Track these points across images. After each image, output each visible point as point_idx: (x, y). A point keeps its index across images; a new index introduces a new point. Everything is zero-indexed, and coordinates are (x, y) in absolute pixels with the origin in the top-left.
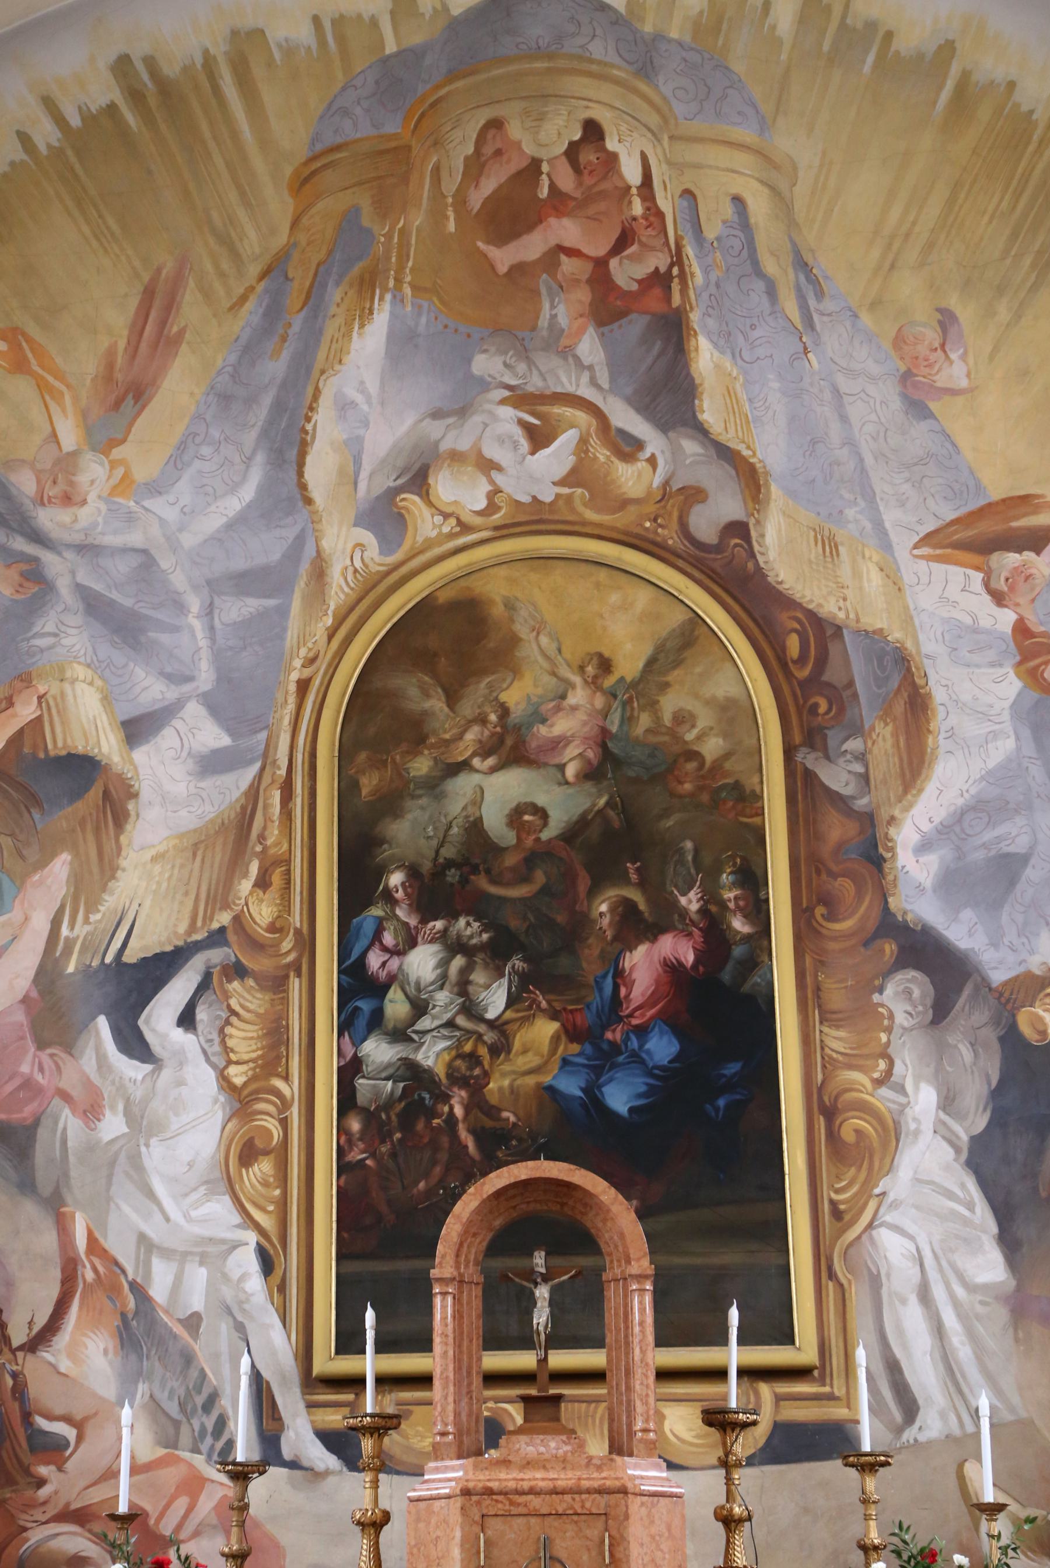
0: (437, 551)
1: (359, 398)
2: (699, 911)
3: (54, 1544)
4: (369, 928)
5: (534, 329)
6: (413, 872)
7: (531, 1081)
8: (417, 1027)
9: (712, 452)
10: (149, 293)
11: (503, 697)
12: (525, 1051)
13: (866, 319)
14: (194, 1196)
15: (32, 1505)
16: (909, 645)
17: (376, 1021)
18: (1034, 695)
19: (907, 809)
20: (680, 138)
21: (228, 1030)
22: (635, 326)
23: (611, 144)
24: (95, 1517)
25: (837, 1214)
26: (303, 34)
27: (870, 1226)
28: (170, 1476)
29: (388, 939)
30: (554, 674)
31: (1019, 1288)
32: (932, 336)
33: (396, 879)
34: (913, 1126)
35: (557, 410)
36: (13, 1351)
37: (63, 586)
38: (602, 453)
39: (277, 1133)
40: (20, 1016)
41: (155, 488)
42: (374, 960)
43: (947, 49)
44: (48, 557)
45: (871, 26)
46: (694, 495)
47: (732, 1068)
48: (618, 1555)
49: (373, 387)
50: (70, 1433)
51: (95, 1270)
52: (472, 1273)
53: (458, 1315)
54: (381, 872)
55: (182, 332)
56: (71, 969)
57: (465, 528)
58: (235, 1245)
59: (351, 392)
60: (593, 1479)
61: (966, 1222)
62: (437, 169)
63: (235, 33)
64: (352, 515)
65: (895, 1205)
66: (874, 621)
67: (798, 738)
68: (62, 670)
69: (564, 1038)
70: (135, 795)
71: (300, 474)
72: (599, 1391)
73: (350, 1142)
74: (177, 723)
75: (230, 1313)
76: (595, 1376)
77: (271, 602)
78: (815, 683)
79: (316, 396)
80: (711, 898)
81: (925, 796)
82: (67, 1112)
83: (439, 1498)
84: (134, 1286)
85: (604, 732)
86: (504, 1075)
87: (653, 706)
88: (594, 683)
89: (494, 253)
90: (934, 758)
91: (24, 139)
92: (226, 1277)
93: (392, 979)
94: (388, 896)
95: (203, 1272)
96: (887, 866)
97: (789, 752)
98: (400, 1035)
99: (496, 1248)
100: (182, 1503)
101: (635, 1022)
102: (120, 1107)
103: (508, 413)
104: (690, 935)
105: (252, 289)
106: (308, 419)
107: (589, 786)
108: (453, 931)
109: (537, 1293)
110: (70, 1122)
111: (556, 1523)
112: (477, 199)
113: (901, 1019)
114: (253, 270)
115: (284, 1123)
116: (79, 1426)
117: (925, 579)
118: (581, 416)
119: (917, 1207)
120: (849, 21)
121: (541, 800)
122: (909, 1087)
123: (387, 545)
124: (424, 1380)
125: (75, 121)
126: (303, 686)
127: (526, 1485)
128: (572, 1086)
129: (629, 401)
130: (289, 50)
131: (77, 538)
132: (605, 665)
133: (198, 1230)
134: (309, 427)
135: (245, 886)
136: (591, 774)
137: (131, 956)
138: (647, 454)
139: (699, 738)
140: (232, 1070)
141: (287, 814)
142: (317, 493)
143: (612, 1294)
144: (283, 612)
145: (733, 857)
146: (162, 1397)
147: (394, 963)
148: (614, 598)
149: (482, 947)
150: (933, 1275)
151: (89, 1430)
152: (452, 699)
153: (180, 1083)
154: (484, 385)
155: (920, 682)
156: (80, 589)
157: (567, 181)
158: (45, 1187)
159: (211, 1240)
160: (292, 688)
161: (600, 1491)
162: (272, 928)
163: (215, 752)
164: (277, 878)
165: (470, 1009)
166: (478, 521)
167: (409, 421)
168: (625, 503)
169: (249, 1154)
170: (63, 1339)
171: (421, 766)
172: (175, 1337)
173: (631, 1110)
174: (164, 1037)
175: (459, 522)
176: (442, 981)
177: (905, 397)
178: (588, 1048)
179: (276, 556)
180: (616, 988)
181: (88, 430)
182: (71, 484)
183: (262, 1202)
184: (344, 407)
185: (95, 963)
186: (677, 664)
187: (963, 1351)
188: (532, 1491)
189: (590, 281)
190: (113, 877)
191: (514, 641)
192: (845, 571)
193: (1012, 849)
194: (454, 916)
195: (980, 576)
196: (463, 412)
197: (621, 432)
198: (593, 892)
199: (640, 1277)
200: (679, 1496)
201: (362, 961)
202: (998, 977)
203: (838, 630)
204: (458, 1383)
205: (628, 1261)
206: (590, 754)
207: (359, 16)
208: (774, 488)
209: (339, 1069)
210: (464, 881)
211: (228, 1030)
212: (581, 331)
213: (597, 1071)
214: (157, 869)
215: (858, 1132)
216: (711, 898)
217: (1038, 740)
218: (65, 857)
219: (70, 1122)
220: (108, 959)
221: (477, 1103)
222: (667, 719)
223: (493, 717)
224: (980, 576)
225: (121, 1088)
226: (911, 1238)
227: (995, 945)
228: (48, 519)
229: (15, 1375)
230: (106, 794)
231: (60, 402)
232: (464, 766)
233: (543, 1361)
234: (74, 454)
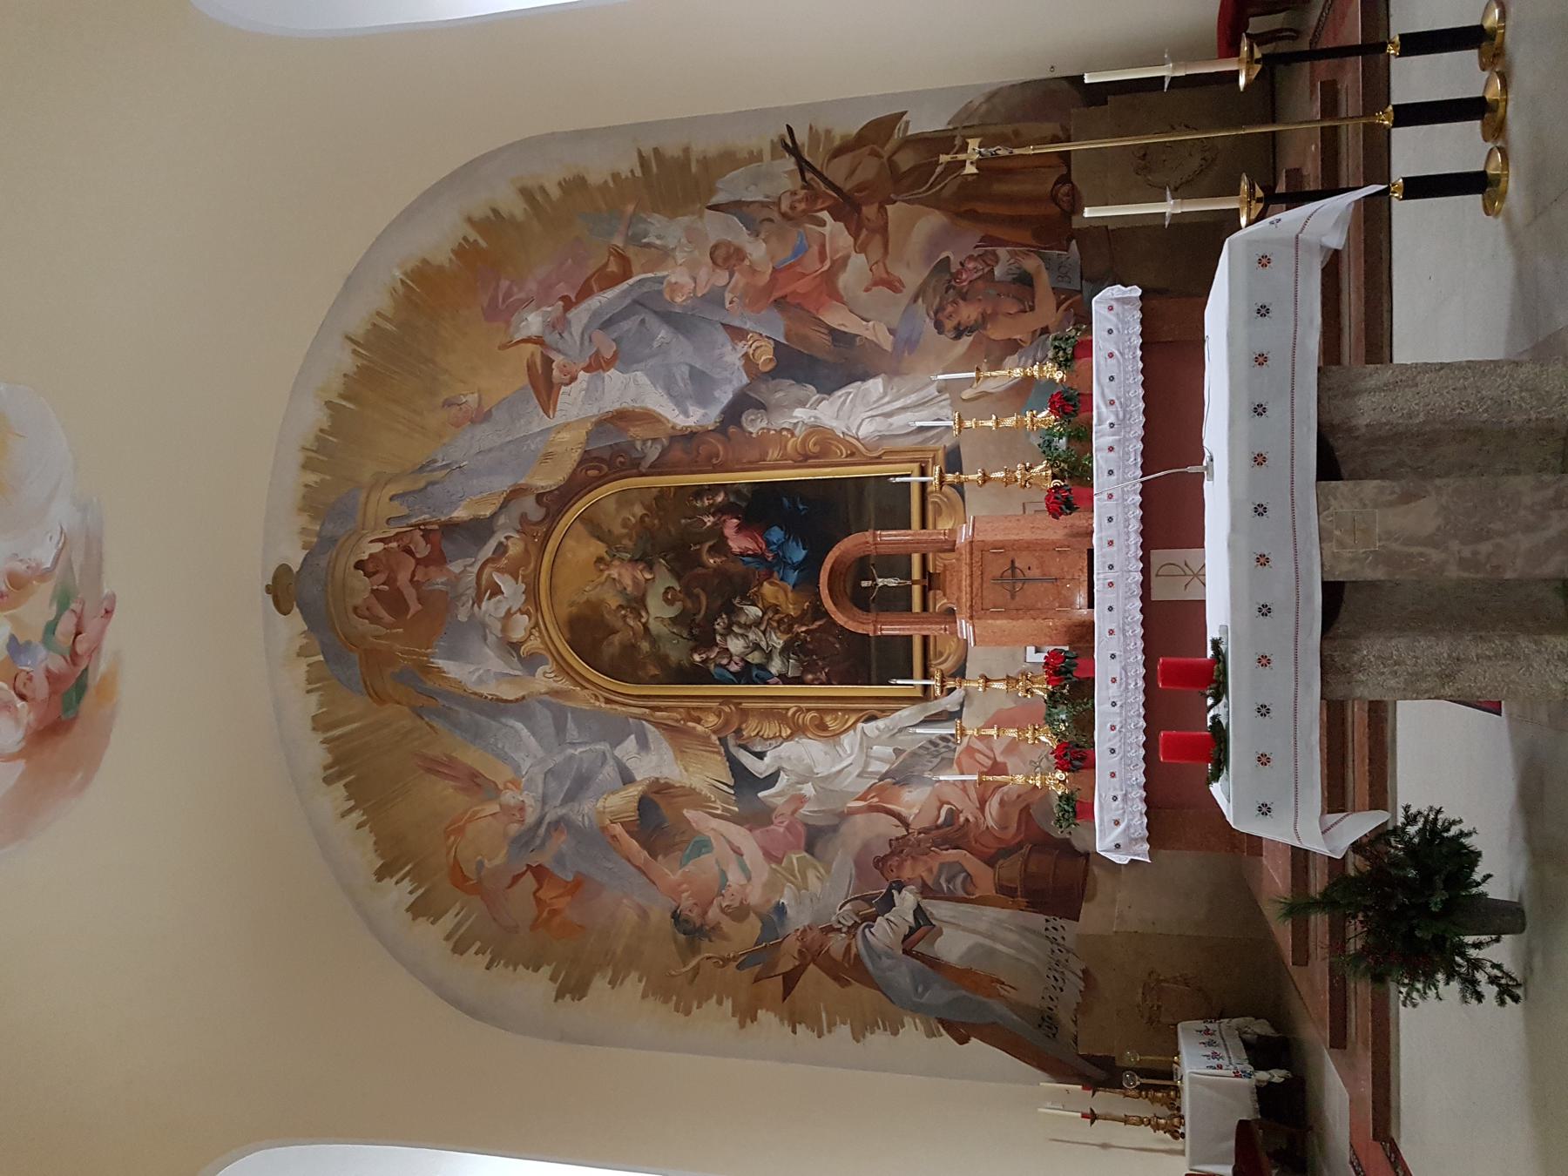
0: (547, 638)
1: (477, 674)
2: (714, 516)
3: (994, 813)
5: (447, 593)
6: (694, 650)
7: (790, 595)
8: (765, 648)
9: (504, 510)
10: (429, 770)
11: (614, 607)
12: (777, 598)
13: (446, 440)
14: (841, 752)
15: (977, 824)
16: (593, 420)
17: (763, 667)
18: (617, 363)
19: (668, 421)
20: (363, 524)
21: (765, 736)
22: (447, 547)
23: (365, 557)
24: (983, 796)
25: (852, 454)
26: (314, 697)
27: (858, 439)
28: (965, 761)
29: (725, 662)
30: (603, 584)
31: (885, 373)
32: (455, 410)
33: (697, 658)
34: (812, 419)
35: (484, 582)
36: (909, 833)
37: (562, 811)
38: (504, 561)
39: (813, 714)
40: (758, 832)
41: (517, 768)
42: (734, 668)
43: (328, 404)
44: (548, 819)
45: (317, 438)
46: (523, 518)
48: (1001, 544)
49: (472, 668)
50: (946, 807)
51: (873, 797)
52: (872, 616)
53: (891, 623)
54: (693, 664)
55: (446, 756)
56: (736, 809)
57: (536, 625)
59: (474, 677)
60: (966, 557)
61: (856, 395)
62: (377, 637)
63: (314, 729)
64: (530, 678)
65: (848, 428)
66: (582, 434)
67: (635, 471)
68: (599, 812)
69: (772, 580)
70: (657, 779)
71: (511, 701)
72: (930, 556)
73: (818, 679)
74: (624, 760)
78: (610, 463)
79: (475, 694)
80: (707, 511)
81: (662, 413)
82: (801, 811)
83: (974, 632)
84: (880, 780)
85: (630, 560)
86: (788, 608)
88: (608, 565)
89: (412, 612)
90: (646, 409)
91: (360, 826)
92: (878, 736)
93: (743, 660)
95: (875, 747)
96: (694, 430)
98: (769, 656)
99: (866, 609)
100: (979, 756)
101: (764, 547)
102: (800, 786)
103: (484, 605)
104: (725, 521)
105: (427, 723)
106: (486, 697)
107: (656, 567)
108: (721, 631)
109: (881, 584)
110: (805, 810)
111: (985, 574)
112: (387, 618)
113: (764, 424)
114: (419, 722)
115: (809, 710)
116: (942, 803)
117: (564, 413)
118: (487, 571)
119: (849, 418)
120: (314, 448)
122: (795, 421)
125: (352, 803)
126: (608, 701)
127: (968, 589)
128: (793, 576)
129: (480, 549)
130: (321, 705)
131: (539, 804)
132: (600, 560)
133: (856, 749)
134: (490, 697)
135: (699, 728)
136: (650, 567)
137: (731, 782)
138: (503, 540)
139: (634, 516)
140: (784, 735)
141: (666, 709)
143: (883, 550)
144: (574, 710)
145: (689, 501)
146: (931, 765)
148: (569, 555)
149: (729, 618)
150: (879, 411)
151: (944, 799)
152: (615, 632)
153: (789, 758)
154: (472, 616)
155: (610, 414)
156: (564, 802)
157: (382, 577)
158: (836, 821)
159: (861, 744)
160: (608, 706)
161: (971, 554)
162: (719, 716)
164: (695, 714)
165: (757, 623)
166: (533, 619)
167: (488, 651)
168: (526, 551)
169: (822, 727)
170: (904, 811)
171: (645, 646)
172: (904, 759)
173: (804, 549)
174: (768, 766)
175: (534, 628)
176: (744, 636)
177: (481, 422)
178: (776, 568)
179: (548, 713)
180: (749, 555)
181: (490, 800)
182: (514, 807)
183: (844, 721)
184: (480, 681)
185: (734, 798)
186: (599, 526)
187: (913, 398)
188: (971, 586)
189: (426, 566)
190: (694, 789)
193: (687, 373)
195: (563, 387)
196: (484, 626)
197: (494, 553)
198: (703, 566)
199: (875, 536)
200: (974, 518)
202: (745, 380)
204: (923, 623)
205: (867, 543)
206: (641, 567)
207: (307, 671)
208: (522, 481)
209: (784, 684)
210: (698, 626)
211: (765, 736)
212: (449, 571)
213: (786, 564)
214: (691, 769)
215: (815, 445)
216: (707, 511)
217: (638, 361)
218: (685, 812)
219: (805, 810)
220: (732, 792)
221: (800, 620)
222: (625, 531)
223: (623, 612)
224: (563, 387)
225: (791, 785)
226: (863, 420)
227: (731, 382)
228: (531, 818)
229: (919, 833)
230: (656, 792)
231: (478, 812)
232: (645, 625)
233: (915, 582)
234: (501, 806)
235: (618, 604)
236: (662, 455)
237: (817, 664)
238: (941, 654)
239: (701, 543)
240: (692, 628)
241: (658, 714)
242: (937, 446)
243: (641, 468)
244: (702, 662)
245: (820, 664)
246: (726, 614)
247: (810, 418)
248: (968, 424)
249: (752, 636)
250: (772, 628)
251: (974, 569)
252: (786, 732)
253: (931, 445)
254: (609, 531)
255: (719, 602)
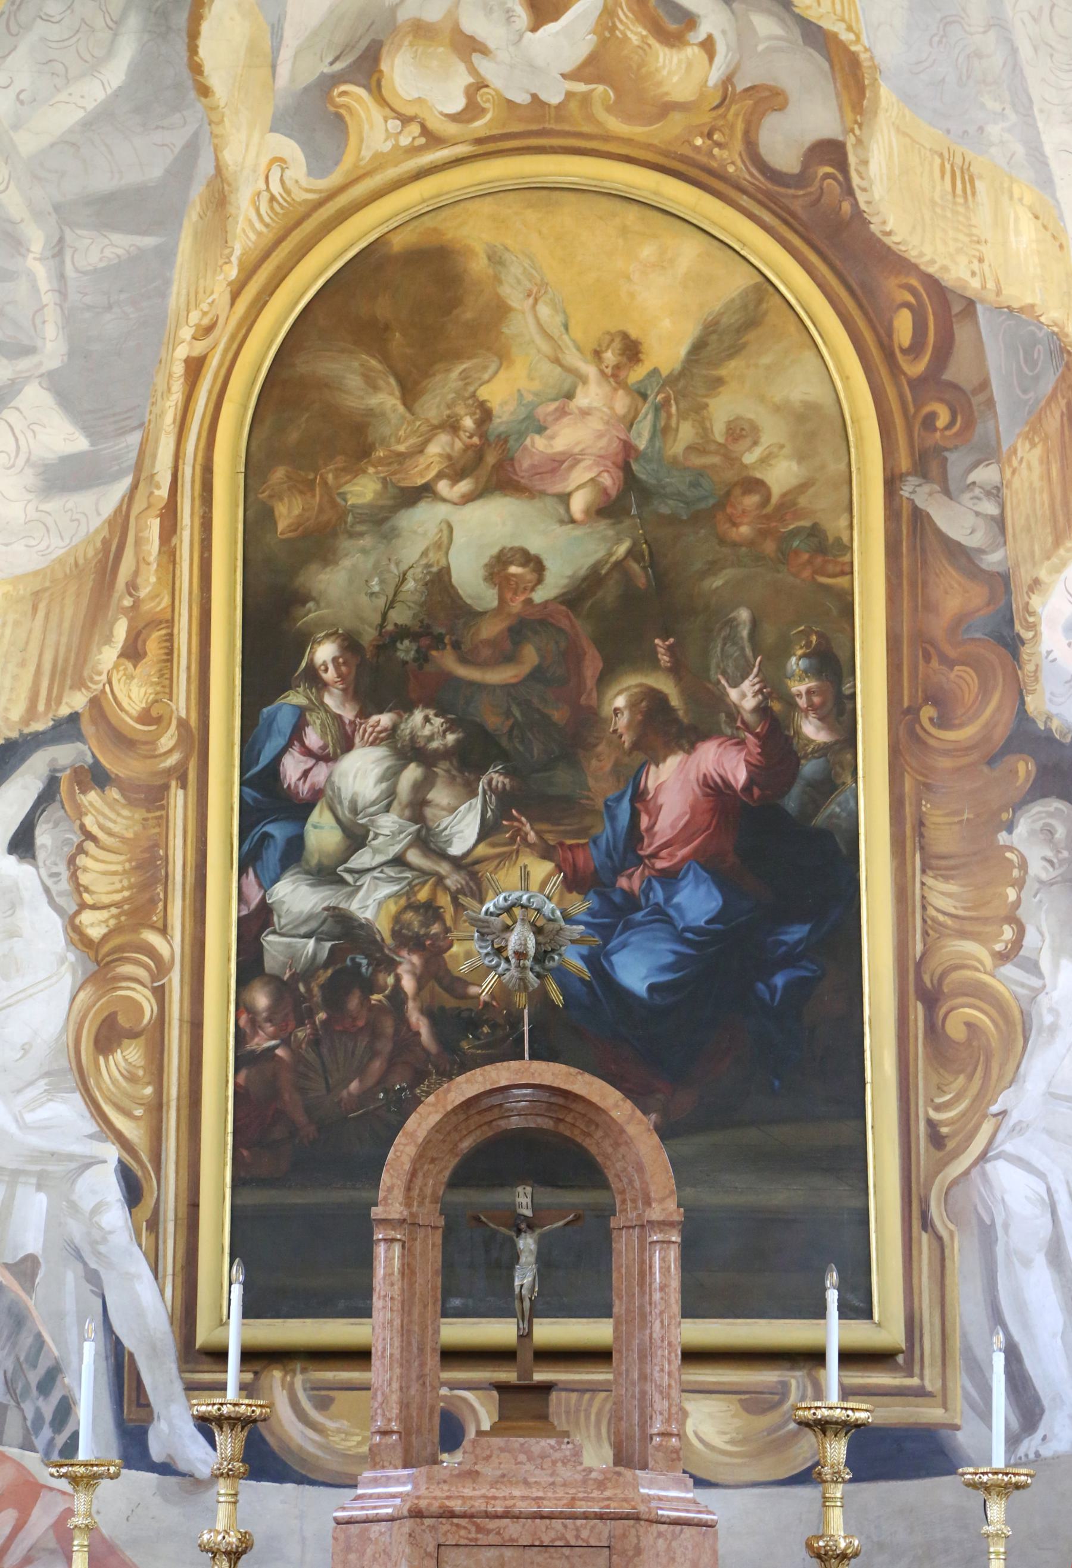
0: (392, 173)
4: (285, 721)
6: (350, 644)
9: (797, 33)
11: (484, 393)
14: (30, 1093)
19: (1058, 569)
21: (81, 860)
25: (937, 1140)
27: (983, 1157)
29: (313, 738)
33: (325, 652)
34: (1048, 1019)
38: (635, 33)
42: (292, 767)
47: (796, 933)
52: (430, 1214)
53: (408, 1271)
54: (303, 641)
57: (432, 139)
58: (89, 1163)
64: (268, 111)
65: (1019, 1129)
66: (1017, 294)
67: (904, 463)
71: (193, 49)
75: (79, 1256)
76: (600, 1356)
77: (149, 241)
83: (378, 1520)
85: (628, 447)
87: (698, 411)
88: (615, 377)
92: (74, 1208)
93: (317, 794)
94: (313, 678)
95: (41, 1199)
96: (1025, 651)
97: (892, 483)
101: (660, 864)
104: (741, 743)
107: (603, 526)
108: (406, 729)
113: (1037, 869)
115: (160, 994)
119: (1050, 1133)
121: (535, 545)
122: (1045, 965)
123: (318, 163)
124: (360, 1356)
126: (195, 367)
132: (632, 350)
133: (35, 1141)
135: (108, 656)
138: (701, 34)
140: (87, 918)
142: (216, 78)
143: (624, 1246)
144: (166, 256)
145: (806, 634)
147: (320, 773)
148: (647, 251)
149: (446, 754)
152: (410, 394)
160: (179, 369)
162: (146, 717)
163: (67, 460)
164: (153, 646)
166: (452, 129)
168: (667, 108)
173: (652, 988)
175: (425, 131)
179: (156, 172)
180: (635, 816)
183: (126, 1103)
186: (735, 350)
191: (501, 310)
192: (983, 215)
194: (406, 707)
198: (606, 678)
199: (664, 1225)
201: (274, 768)
203: (970, 305)
205: (648, 1202)
208: (884, 91)
209: (240, 920)
210: (423, 657)
211: (81, 860)
213: (606, 932)
215: (969, 1025)
222: (718, 431)
223: (468, 423)
226: (1041, 1175)
232: (426, 491)
233: (525, 1336)
235: (495, 404)
236: (955, 551)
237: (300, 1023)
238: (323, 1405)
239: (676, 670)
240: (414, 636)
241: (154, 527)
242: (958, 1402)
243: (913, 480)
244: (311, 666)
245: (301, 1034)
246: (458, 741)
247: (1051, 1010)
248: (997, 1510)
249: (388, 823)
250: (411, 890)
251: (557, 1524)
252: (94, 925)
253: (961, 1382)
254: (719, 381)
255: (493, 721)
